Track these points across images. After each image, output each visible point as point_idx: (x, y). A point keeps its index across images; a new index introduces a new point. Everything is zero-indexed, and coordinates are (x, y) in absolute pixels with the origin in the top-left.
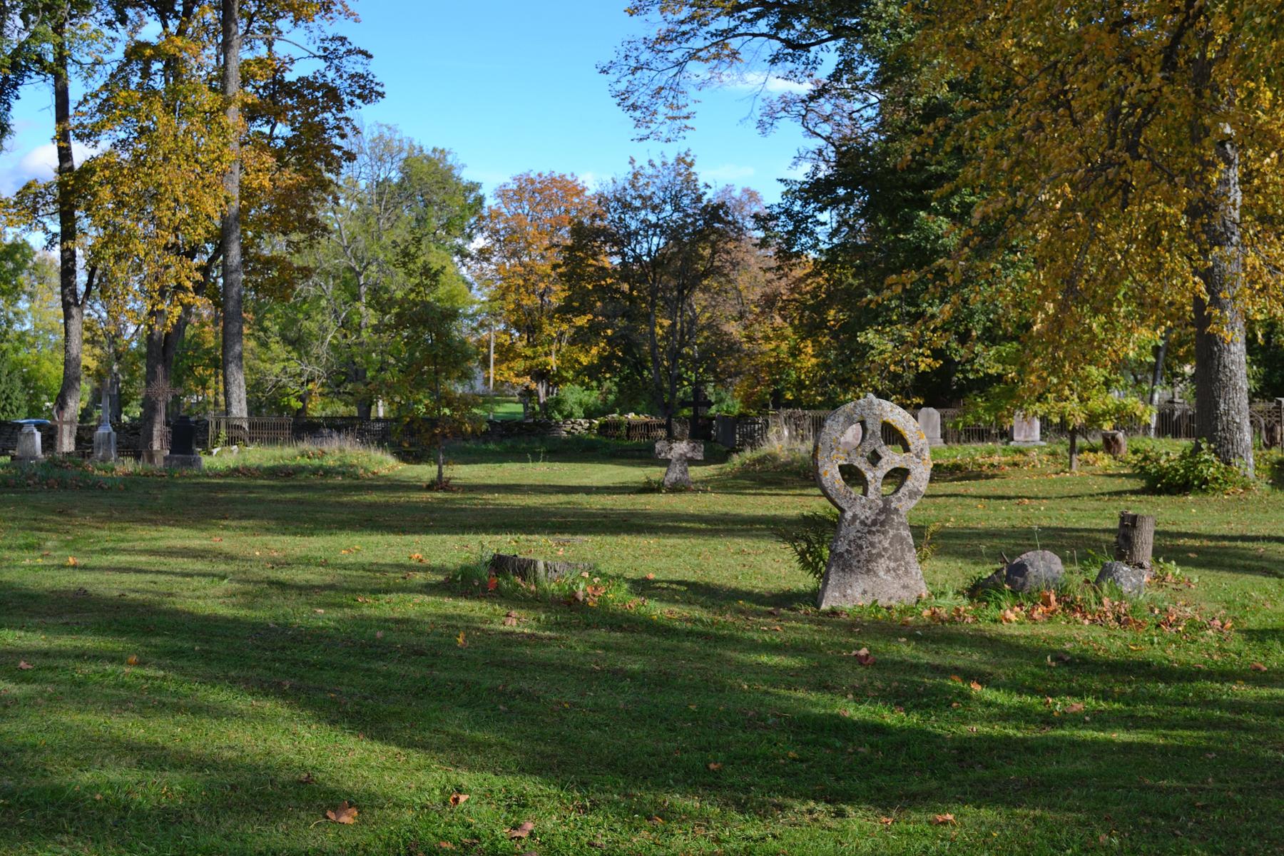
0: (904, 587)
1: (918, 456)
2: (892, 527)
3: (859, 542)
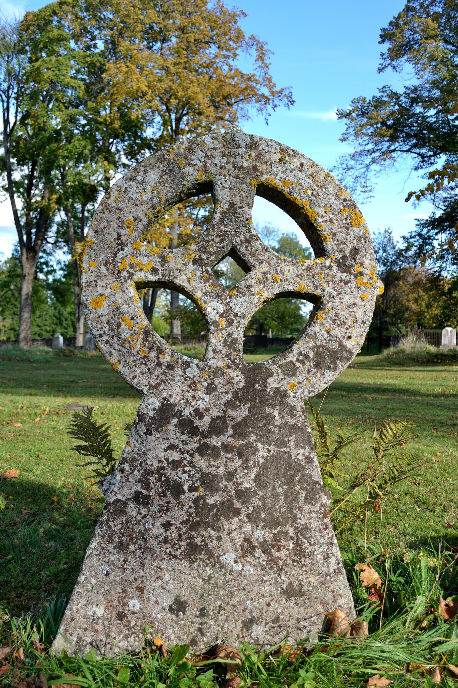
0: (290, 593)
1: (343, 265)
2: (264, 438)
3: (173, 475)
